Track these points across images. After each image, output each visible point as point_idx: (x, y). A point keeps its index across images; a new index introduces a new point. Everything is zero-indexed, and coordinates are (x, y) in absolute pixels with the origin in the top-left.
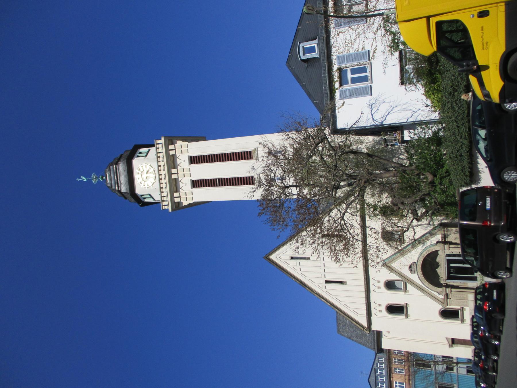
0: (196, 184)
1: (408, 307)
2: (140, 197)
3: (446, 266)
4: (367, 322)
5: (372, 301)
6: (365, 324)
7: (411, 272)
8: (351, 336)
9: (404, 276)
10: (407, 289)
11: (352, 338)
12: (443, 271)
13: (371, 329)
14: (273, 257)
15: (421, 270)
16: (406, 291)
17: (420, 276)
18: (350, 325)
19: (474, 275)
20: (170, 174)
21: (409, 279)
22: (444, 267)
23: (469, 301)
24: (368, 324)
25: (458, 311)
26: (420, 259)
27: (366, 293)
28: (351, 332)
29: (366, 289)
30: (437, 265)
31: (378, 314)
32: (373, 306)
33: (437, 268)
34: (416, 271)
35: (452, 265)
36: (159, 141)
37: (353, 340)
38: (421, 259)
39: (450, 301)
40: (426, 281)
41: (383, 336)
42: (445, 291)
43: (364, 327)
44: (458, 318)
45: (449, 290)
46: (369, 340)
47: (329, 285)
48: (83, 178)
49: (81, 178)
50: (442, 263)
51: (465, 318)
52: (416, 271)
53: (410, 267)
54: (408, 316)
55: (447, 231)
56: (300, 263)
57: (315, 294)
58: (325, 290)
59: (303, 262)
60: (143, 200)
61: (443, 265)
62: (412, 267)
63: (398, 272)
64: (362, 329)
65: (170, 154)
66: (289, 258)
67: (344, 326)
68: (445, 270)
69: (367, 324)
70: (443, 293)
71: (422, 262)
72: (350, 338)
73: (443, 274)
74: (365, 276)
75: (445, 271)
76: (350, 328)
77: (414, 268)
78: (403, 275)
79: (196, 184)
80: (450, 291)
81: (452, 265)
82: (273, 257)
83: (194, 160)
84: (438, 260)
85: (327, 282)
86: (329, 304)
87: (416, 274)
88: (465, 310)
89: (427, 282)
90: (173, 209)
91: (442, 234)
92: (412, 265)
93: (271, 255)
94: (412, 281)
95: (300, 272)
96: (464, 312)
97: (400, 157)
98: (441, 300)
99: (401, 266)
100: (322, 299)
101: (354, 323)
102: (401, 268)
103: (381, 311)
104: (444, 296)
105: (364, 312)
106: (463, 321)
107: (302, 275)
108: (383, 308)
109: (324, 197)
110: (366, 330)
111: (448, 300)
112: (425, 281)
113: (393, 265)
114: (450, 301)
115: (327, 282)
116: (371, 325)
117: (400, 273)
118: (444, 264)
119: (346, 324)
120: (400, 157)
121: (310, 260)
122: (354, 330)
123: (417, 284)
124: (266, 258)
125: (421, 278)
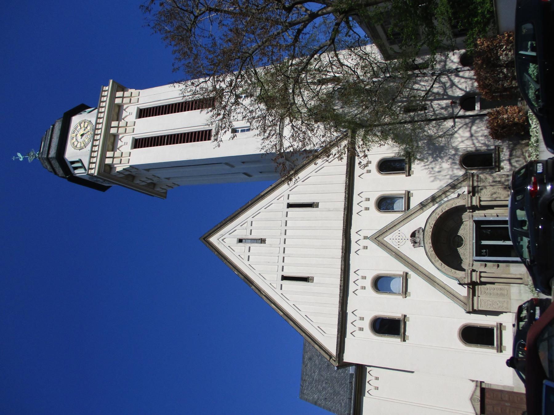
0: (139, 143)
1: (407, 322)
2: (69, 164)
3: (474, 241)
4: (337, 345)
5: (349, 310)
6: (333, 349)
8: (318, 399)
9: (403, 256)
10: (409, 291)
11: (319, 402)
12: (468, 251)
13: (343, 359)
14: (213, 240)
15: (430, 241)
16: (406, 294)
17: (428, 251)
18: (319, 380)
19: (521, 173)
20: (108, 127)
21: (410, 262)
22: (471, 243)
24: (338, 348)
25: (493, 329)
26: (429, 221)
27: (341, 295)
28: (320, 392)
29: (342, 287)
30: (459, 242)
31: (358, 333)
32: (350, 318)
35: (484, 242)
36: (107, 88)
37: (320, 405)
38: (432, 222)
40: (437, 258)
41: (366, 394)
42: (469, 275)
43: (331, 356)
44: (492, 344)
46: (343, 400)
47: (286, 283)
48: (19, 155)
49: (18, 157)
50: (468, 238)
51: (504, 344)
53: (413, 235)
54: (406, 338)
55: (478, 181)
56: (250, 247)
57: (263, 297)
58: (279, 292)
59: (256, 247)
60: (72, 170)
61: (468, 240)
62: (417, 235)
63: (394, 250)
64: (328, 358)
65: (116, 103)
66: (235, 240)
67: (310, 383)
68: (471, 249)
69: (337, 352)
72: (316, 403)
73: (468, 257)
74: (343, 267)
75: (471, 251)
76: (318, 385)
77: (419, 237)
78: (401, 255)
79: (139, 143)
81: (484, 242)
82: (213, 240)
83: (143, 113)
84: (461, 233)
85: (284, 278)
86: (281, 314)
88: (505, 330)
89: (440, 261)
90: (101, 172)
91: (469, 186)
92: (417, 233)
93: (213, 235)
94: (414, 264)
95: (247, 263)
96: (504, 332)
97: (414, 86)
98: (462, 299)
99: (399, 241)
100: (273, 305)
101: (316, 346)
102: (399, 243)
105: (334, 331)
106: (500, 349)
107: (249, 266)
108: (366, 324)
109: (282, 85)
110: (335, 361)
111: (475, 298)
112: (439, 262)
115: (284, 278)
116: (343, 352)
117: (397, 252)
118: (471, 239)
119: (313, 379)
120: (414, 86)
121: (265, 243)
122: (323, 388)
123: (422, 270)
124: (204, 239)
125: (429, 254)
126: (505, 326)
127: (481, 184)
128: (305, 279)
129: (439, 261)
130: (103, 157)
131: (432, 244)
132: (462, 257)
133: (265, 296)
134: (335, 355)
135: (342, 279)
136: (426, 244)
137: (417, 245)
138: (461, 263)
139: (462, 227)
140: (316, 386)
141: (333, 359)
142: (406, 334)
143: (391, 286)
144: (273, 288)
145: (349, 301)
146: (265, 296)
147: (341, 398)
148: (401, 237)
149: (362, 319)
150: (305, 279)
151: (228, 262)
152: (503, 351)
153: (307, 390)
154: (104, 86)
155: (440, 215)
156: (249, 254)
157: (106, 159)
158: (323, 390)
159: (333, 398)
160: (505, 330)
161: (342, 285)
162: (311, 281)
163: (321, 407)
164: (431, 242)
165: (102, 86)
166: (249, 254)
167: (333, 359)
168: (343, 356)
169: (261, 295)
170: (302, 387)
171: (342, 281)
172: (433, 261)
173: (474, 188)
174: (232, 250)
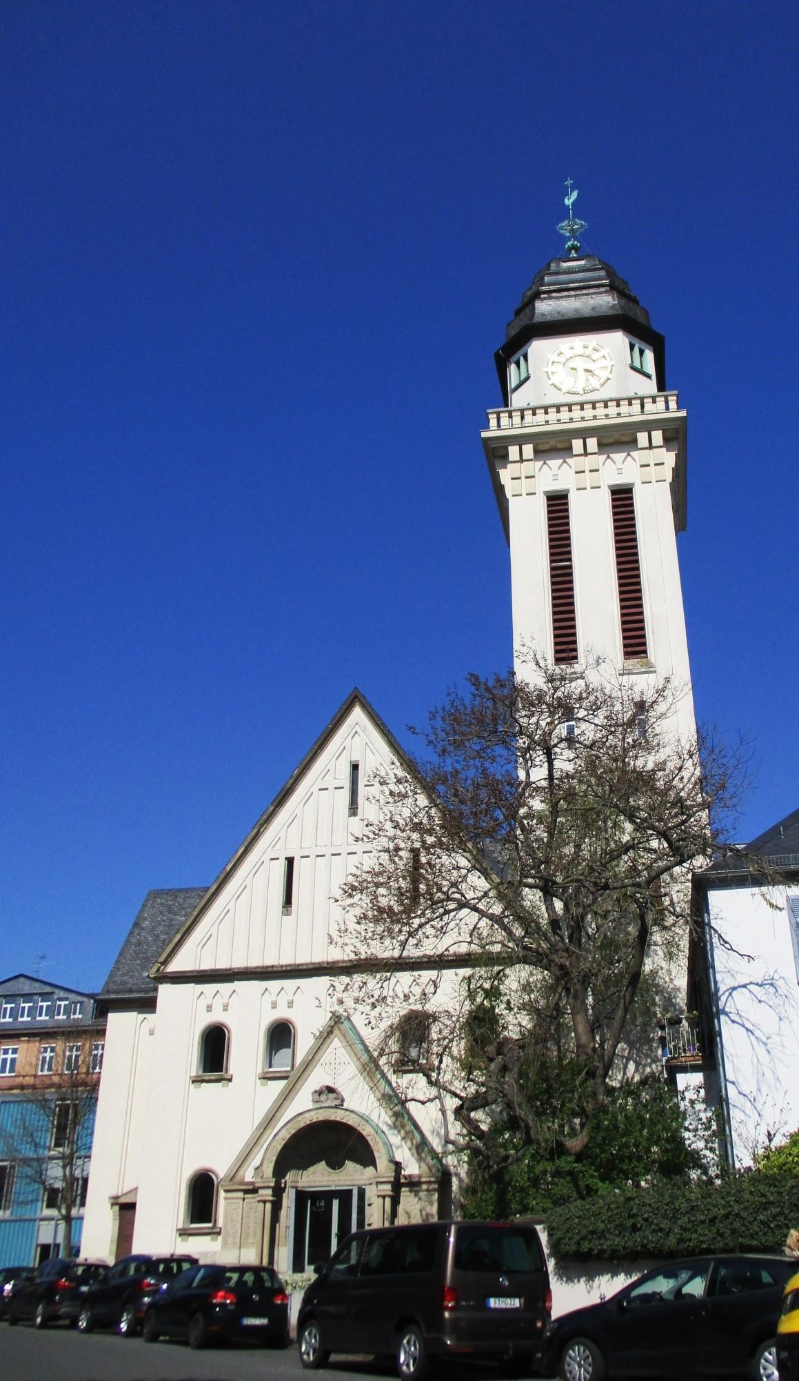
1: (220, 1084)
2: (521, 352)
3: (333, 1188)
5: (238, 985)
6: (175, 966)
7: (316, 1092)
9: (307, 1073)
14: (357, 715)
15: (321, 1118)
16: (264, 1078)
19: (309, 1263)
20: (584, 434)
21: (298, 1086)
22: (330, 1183)
23: (237, 1251)
25: (209, 1221)
26: (353, 1115)
29: (270, 970)
30: (336, 1164)
35: (336, 1203)
37: (131, 933)
38: (351, 1120)
39: (237, 1198)
41: (142, 1016)
42: (266, 1185)
43: (166, 962)
47: (281, 866)
48: (574, 195)
49: (572, 192)
51: (191, 1239)
52: (318, 1105)
53: (330, 1090)
55: (428, 1190)
57: (256, 830)
58: (266, 858)
60: (514, 358)
62: (331, 1095)
63: (317, 1057)
64: (162, 959)
68: (321, 1184)
72: (136, 925)
74: (304, 967)
75: (318, 1184)
76: (164, 926)
77: (327, 1099)
79: (558, 505)
81: (336, 1203)
82: (357, 715)
83: (622, 498)
84: (350, 1165)
85: (290, 862)
86: (228, 868)
87: (310, 1106)
88: (212, 1240)
89: (288, 1136)
90: (489, 442)
91: (420, 1176)
95: (315, 789)
97: (632, 1062)
98: (240, 1173)
101: (178, 936)
102: (328, 1063)
105: (207, 964)
106: (184, 1233)
110: (158, 970)
111: (241, 1194)
114: (237, 1198)
115: (290, 862)
116: (173, 983)
118: (336, 1183)
119: (175, 914)
120: (632, 1062)
121: (350, 816)
122: (157, 936)
124: (356, 697)
125: (300, 1118)
126: (187, 1240)
127: (422, 1194)
128: (288, 901)
129: (289, 1136)
130: (520, 440)
131: (316, 1122)
132: (311, 1169)
133: (259, 831)
134: (168, 971)
135: (284, 969)
136: (315, 1112)
137: (316, 1097)
138: (299, 1168)
139: (358, 1166)
140: (164, 921)
141: (160, 967)
142: (203, 1084)
143: (284, 1050)
144: (273, 843)
145: (252, 982)
146: (259, 831)
147: (136, 973)
148: (338, 1067)
149: (226, 1007)
150: (288, 901)
151: (316, 752)
152: (180, 1238)
153: (161, 904)
154: (677, 395)
155: (362, 1132)
156: (331, 788)
157: (518, 447)
158: (155, 935)
159: (138, 958)
160: (212, 1240)
161: (275, 969)
162: (285, 912)
163: (129, 936)
164: (320, 1119)
165: (676, 392)
166: (331, 788)
167: (160, 967)
168: (167, 982)
169: (258, 826)
170: (167, 893)
171: (280, 969)
172: (289, 1125)
173: (419, 1183)
174: (337, 755)
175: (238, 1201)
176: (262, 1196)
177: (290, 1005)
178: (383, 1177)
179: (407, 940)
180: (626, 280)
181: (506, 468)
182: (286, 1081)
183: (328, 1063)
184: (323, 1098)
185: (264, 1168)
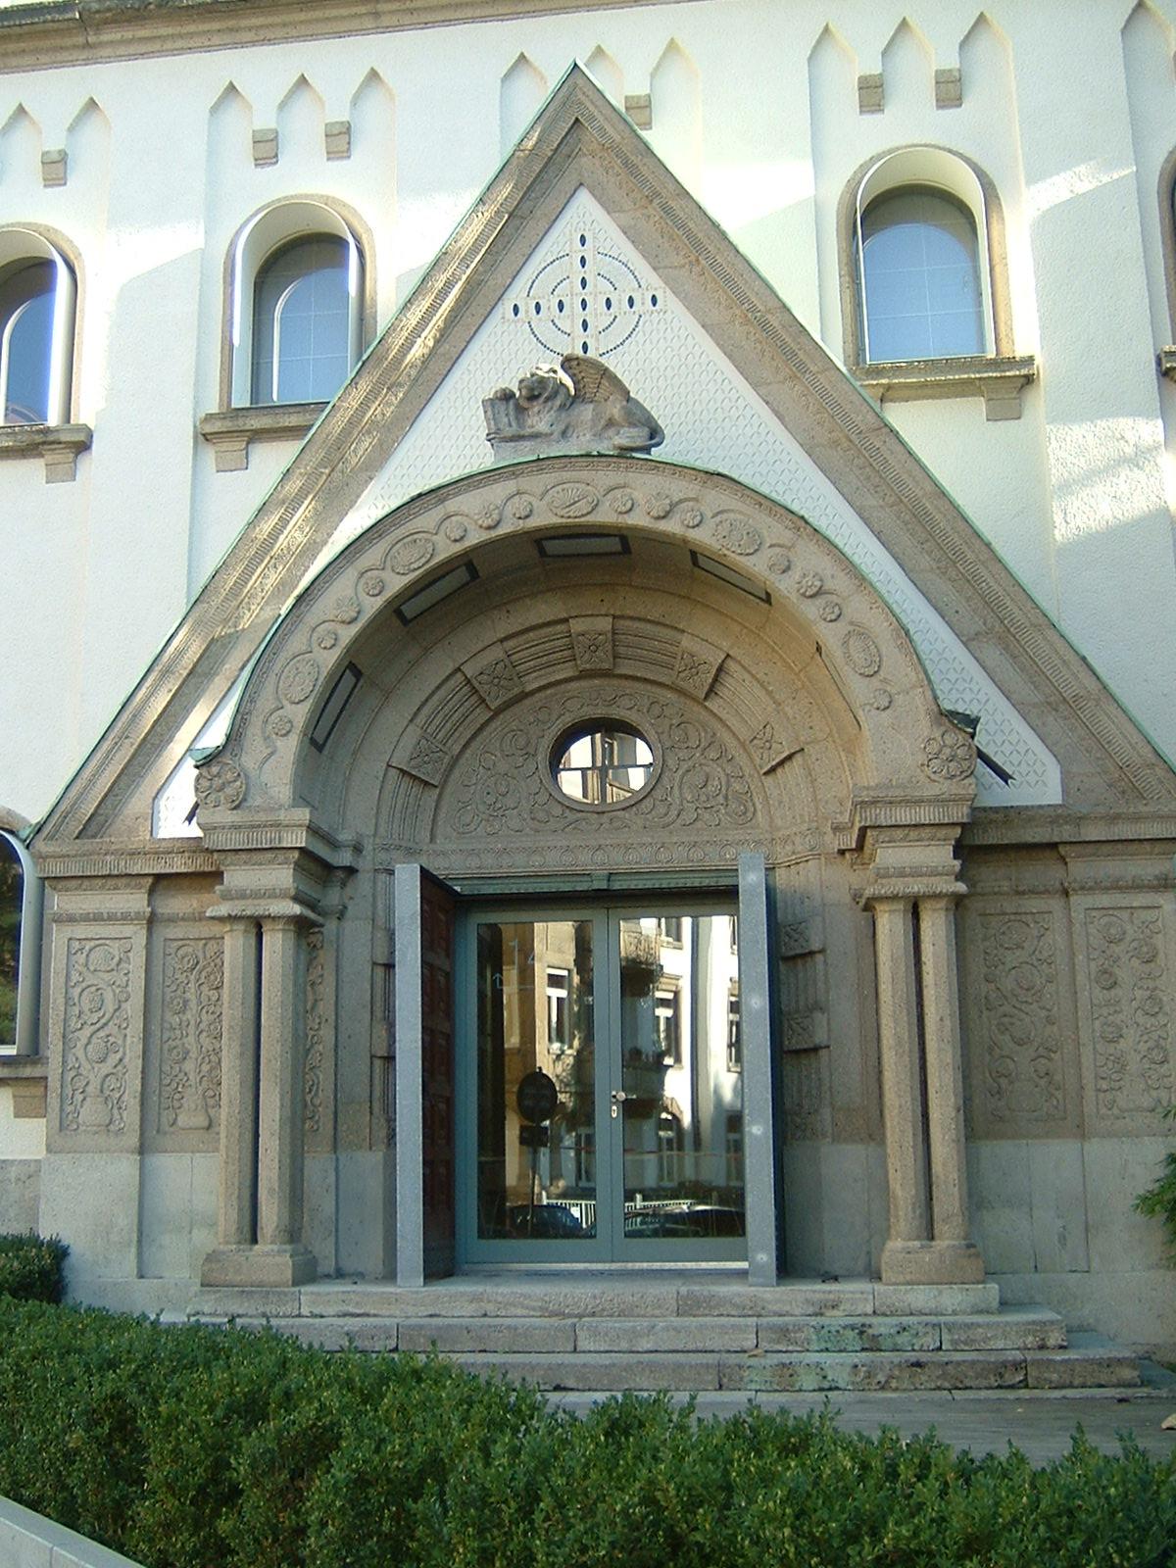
7: (506, 396)
17: (452, 505)
23: (125, 1168)
26: (715, 499)
33: (647, 125)
34: (526, 452)
39: (125, 918)
45: (272, 894)
52: (526, 452)
70: (225, 816)
71: (672, 527)
80: (252, 908)
81: (616, 764)
87: (485, 458)
99: (596, 305)
102: (550, 304)
103: (878, 108)
104: (193, 846)
113: (585, 213)
114: (125, 918)
125: (427, 520)
148: (597, 315)
172: (373, 555)
175: (128, 930)
176: (242, 895)
177: (265, 149)
178: (919, 802)
179: (721, 649)
180: (359, 667)
181: (955, 858)
182: (298, 445)
183: (550, 304)
184: (540, 420)
185: (250, 757)
